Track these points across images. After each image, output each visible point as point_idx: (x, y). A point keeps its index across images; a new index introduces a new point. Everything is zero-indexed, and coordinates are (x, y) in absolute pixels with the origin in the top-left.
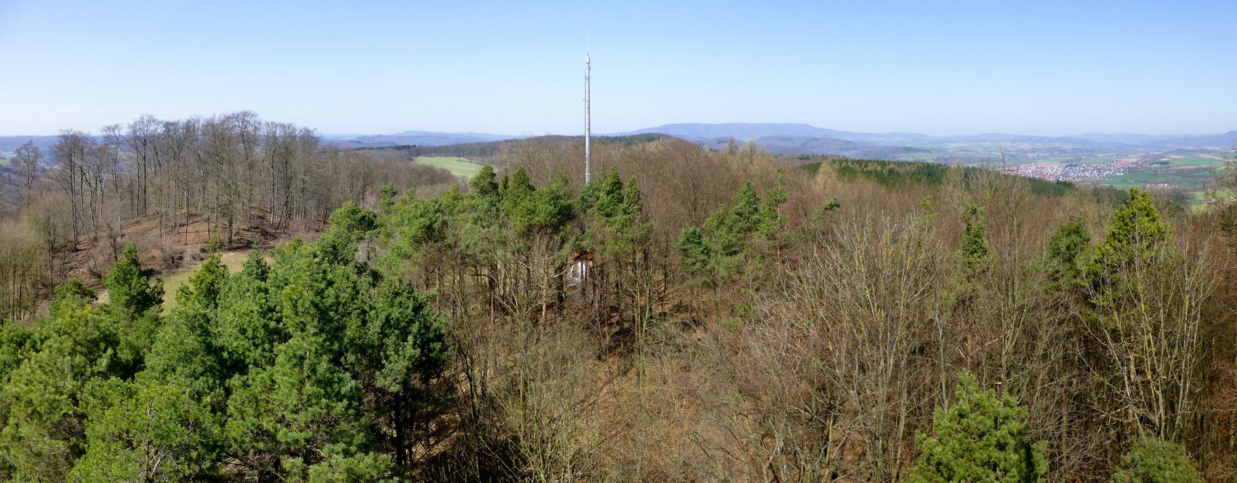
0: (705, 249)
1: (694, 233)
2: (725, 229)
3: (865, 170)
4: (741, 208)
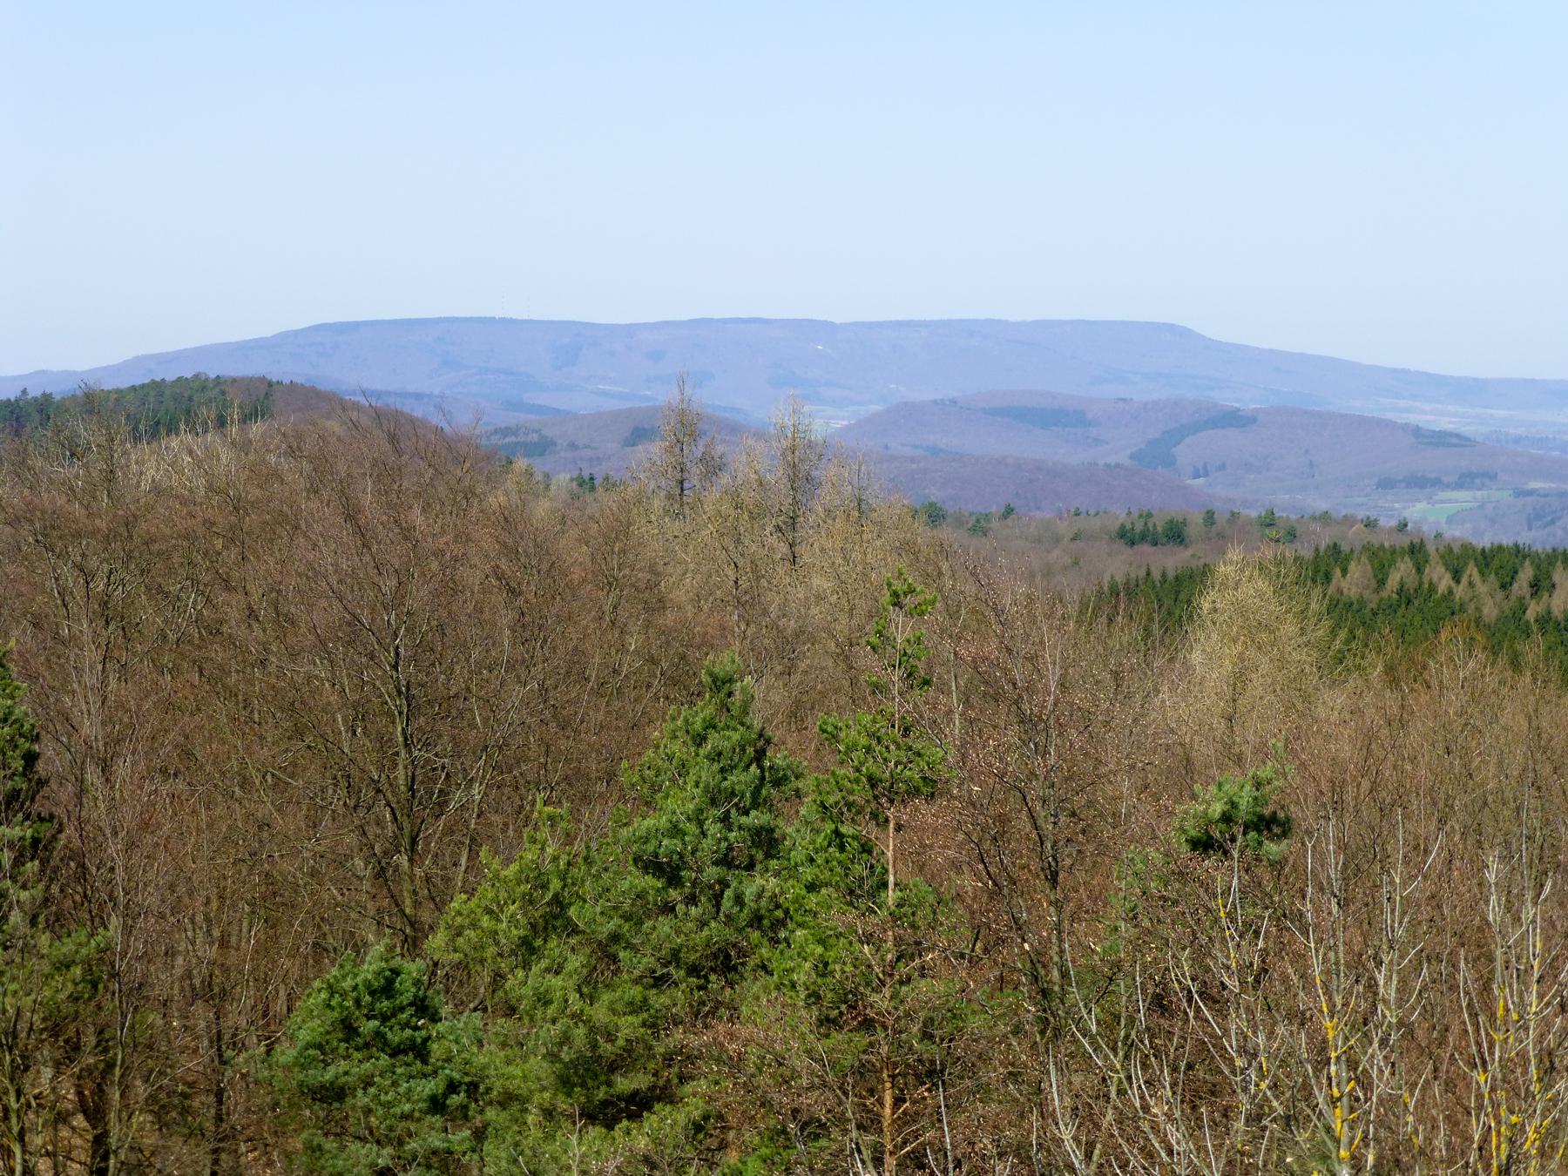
0: (452, 1087)
1: (387, 989)
2: (575, 962)
3: (1533, 611)
4: (675, 831)
